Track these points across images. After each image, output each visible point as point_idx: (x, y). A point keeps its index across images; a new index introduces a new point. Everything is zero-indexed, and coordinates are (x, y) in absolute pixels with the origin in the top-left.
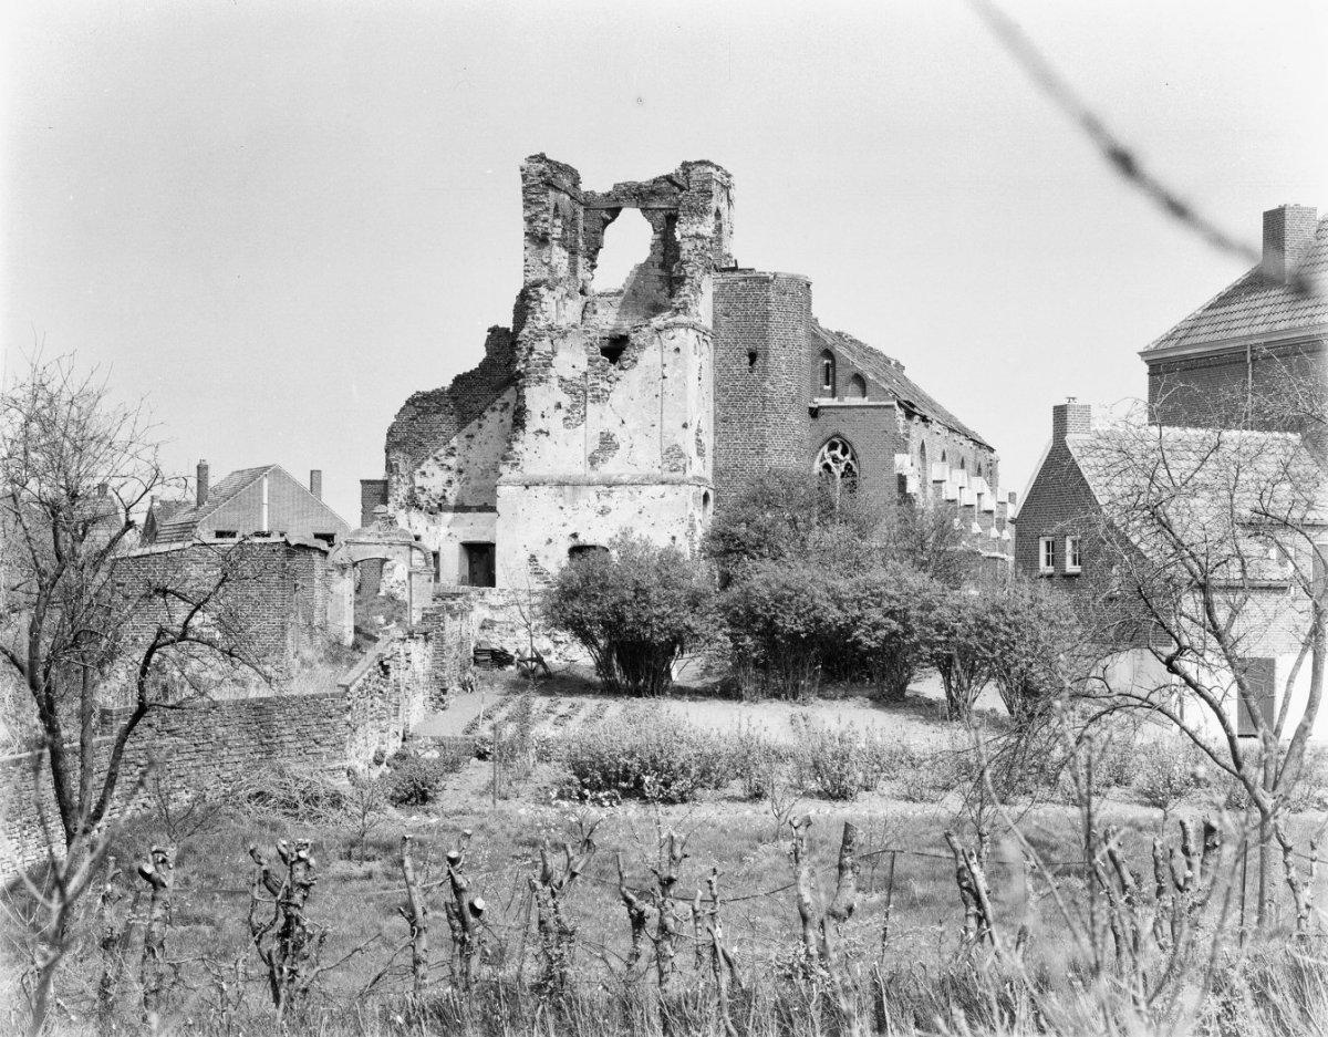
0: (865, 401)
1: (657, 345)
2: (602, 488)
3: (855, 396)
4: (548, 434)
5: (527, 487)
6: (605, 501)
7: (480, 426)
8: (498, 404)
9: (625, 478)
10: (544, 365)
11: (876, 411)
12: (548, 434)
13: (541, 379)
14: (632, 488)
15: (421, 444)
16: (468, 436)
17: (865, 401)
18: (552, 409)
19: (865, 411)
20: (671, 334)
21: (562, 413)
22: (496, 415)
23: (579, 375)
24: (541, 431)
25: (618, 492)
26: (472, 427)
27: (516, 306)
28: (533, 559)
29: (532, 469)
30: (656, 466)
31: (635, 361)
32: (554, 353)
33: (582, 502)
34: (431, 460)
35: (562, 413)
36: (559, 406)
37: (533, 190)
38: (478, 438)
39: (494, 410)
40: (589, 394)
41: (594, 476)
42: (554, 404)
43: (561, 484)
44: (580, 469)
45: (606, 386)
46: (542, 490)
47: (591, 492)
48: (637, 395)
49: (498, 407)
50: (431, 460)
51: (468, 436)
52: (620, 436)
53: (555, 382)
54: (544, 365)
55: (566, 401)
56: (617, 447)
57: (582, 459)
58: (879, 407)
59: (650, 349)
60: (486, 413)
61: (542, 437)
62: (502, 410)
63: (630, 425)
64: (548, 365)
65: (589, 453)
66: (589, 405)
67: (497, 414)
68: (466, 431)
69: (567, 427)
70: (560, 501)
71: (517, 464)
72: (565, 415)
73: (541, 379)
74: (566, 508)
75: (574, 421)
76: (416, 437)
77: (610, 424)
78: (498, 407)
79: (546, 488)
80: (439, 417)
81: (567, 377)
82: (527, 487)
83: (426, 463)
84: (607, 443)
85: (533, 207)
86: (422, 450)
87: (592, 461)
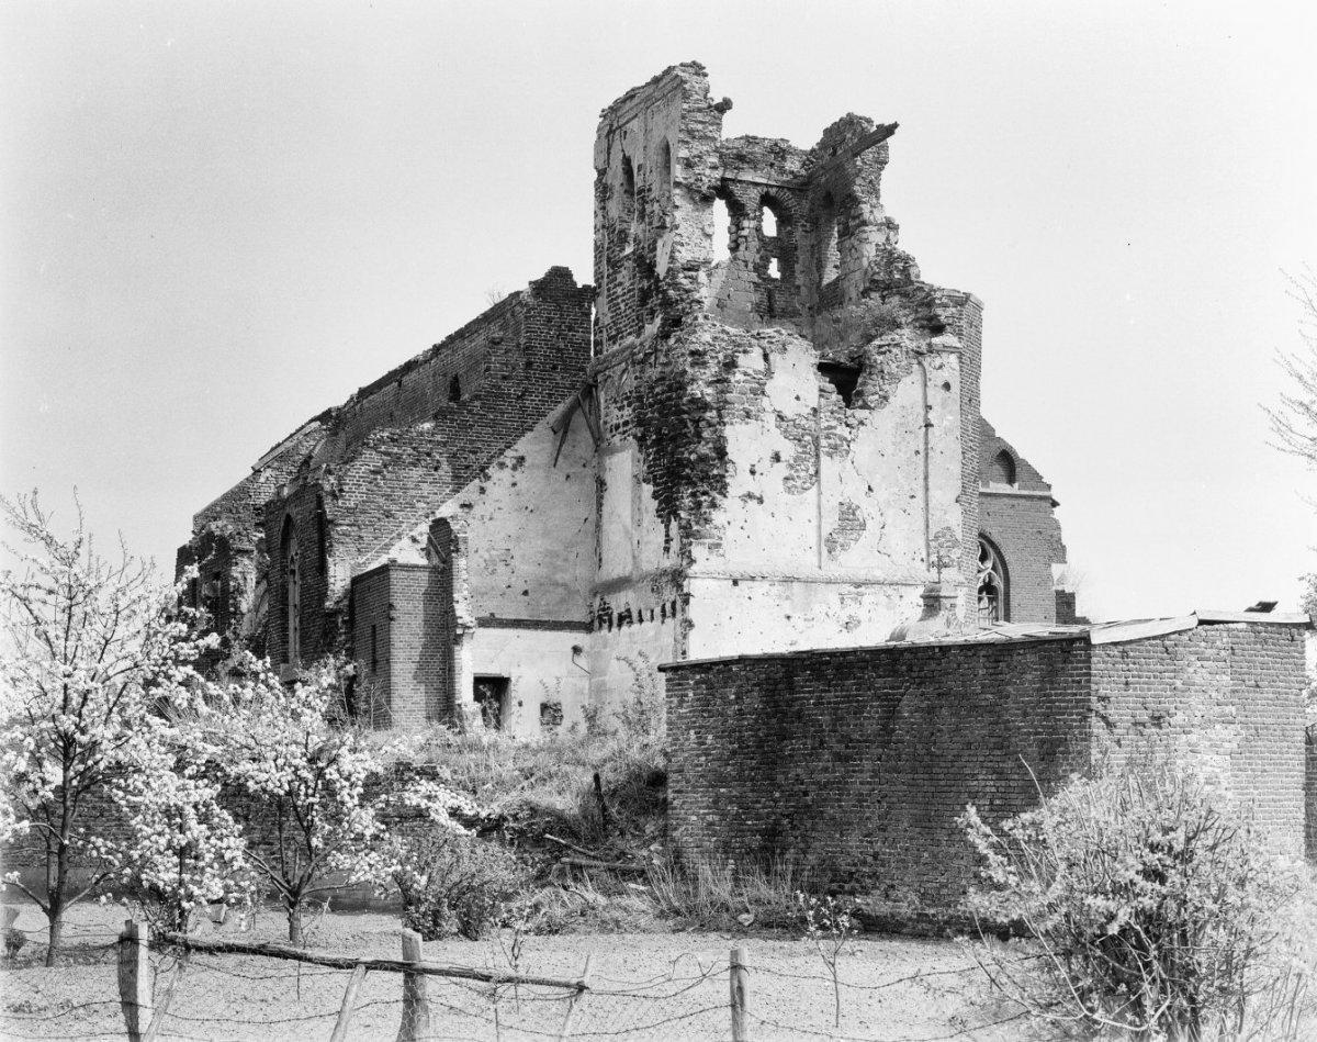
0: (1015, 489)
1: (916, 376)
2: (847, 588)
3: (998, 481)
4: (761, 501)
5: (735, 583)
6: (852, 609)
7: (482, 491)
8: (509, 456)
9: (879, 575)
10: (753, 391)
11: (1028, 503)
12: (761, 501)
13: (748, 415)
14: (889, 590)
15: (388, 515)
16: (463, 506)
17: (1004, 488)
18: (767, 461)
19: (1015, 502)
20: (938, 362)
21: (781, 470)
22: (506, 474)
23: (806, 411)
24: (750, 496)
25: (870, 596)
26: (470, 492)
27: (461, 329)
28: (520, 677)
29: (738, 556)
30: (918, 559)
31: (886, 398)
32: (769, 373)
33: (818, 609)
34: (406, 541)
35: (781, 470)
36: (777, 458)
37: (699, 116)
38: (477, 511)
39: (502, 465)
40: (824, 442)
41: (832, 569)
42: (770, 454)
43: (788, 580)
44: (807, 563)
45: (842, 431)
46: (760, 588)
47: (831, 595)
48: (889, 450)
49: (509, 462)
50: (406, 541)
51: (463, 506)
52: (867, 508)
53: (771, 419)
54: (753, 391)
55: (788, 450)
56: (863, 526)
57: (813, 540)
58: (1030, 498)
59: (907, 380)
60: (490, 471)
61: (753, 504)
62: (514, 468)
63: (881, 494)
64: (760, 391)
65: (825, 534)
66: (824, 459)
67: (507, 472)
68: (463, 496)
69: (789, 490)
70: (787, 608)
71: (718, 546)
72: (787, 473)
73: (748, 415)
74: (795, 616)
75: (799, 483)
76: (382, 501)
77: (854, 492)
78: (509, 462)
79: (765, 585)
80: (416, 473)
81: (788, 413)
82: (735, 583)
83: (398, 544)
84: (850, 519)
85: (695, 144)
86: (389, 524)
87: (831, 545)
